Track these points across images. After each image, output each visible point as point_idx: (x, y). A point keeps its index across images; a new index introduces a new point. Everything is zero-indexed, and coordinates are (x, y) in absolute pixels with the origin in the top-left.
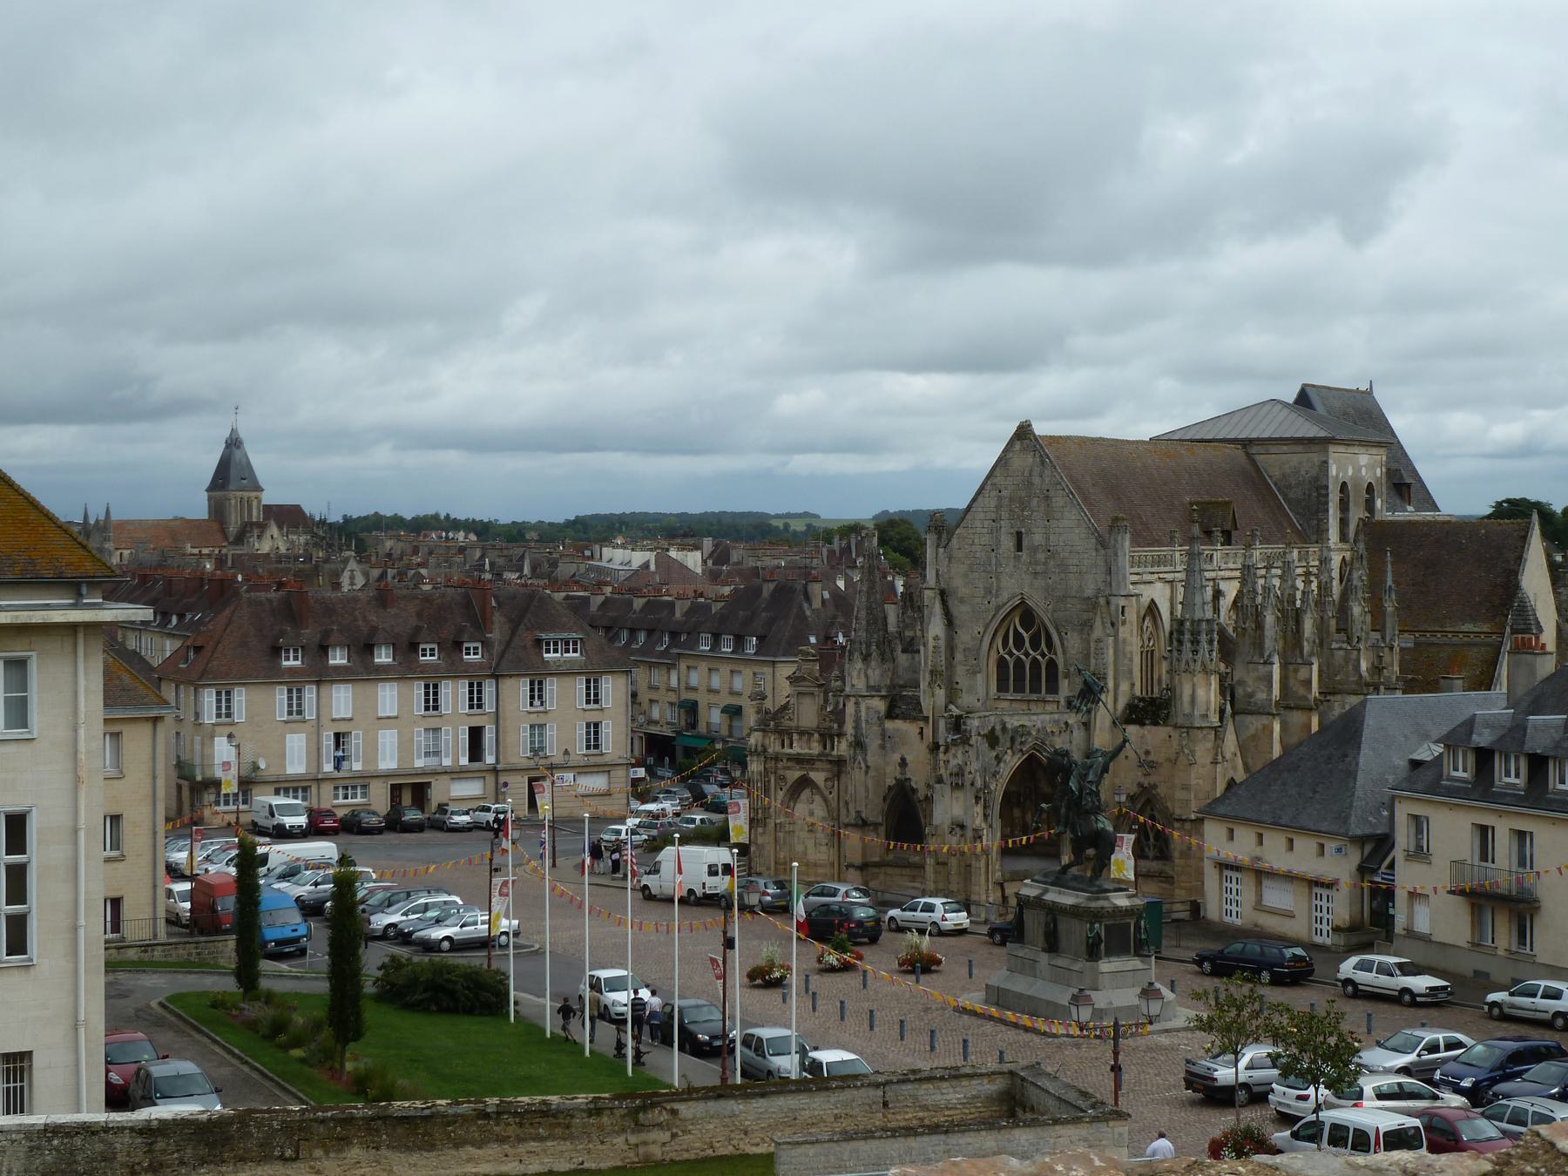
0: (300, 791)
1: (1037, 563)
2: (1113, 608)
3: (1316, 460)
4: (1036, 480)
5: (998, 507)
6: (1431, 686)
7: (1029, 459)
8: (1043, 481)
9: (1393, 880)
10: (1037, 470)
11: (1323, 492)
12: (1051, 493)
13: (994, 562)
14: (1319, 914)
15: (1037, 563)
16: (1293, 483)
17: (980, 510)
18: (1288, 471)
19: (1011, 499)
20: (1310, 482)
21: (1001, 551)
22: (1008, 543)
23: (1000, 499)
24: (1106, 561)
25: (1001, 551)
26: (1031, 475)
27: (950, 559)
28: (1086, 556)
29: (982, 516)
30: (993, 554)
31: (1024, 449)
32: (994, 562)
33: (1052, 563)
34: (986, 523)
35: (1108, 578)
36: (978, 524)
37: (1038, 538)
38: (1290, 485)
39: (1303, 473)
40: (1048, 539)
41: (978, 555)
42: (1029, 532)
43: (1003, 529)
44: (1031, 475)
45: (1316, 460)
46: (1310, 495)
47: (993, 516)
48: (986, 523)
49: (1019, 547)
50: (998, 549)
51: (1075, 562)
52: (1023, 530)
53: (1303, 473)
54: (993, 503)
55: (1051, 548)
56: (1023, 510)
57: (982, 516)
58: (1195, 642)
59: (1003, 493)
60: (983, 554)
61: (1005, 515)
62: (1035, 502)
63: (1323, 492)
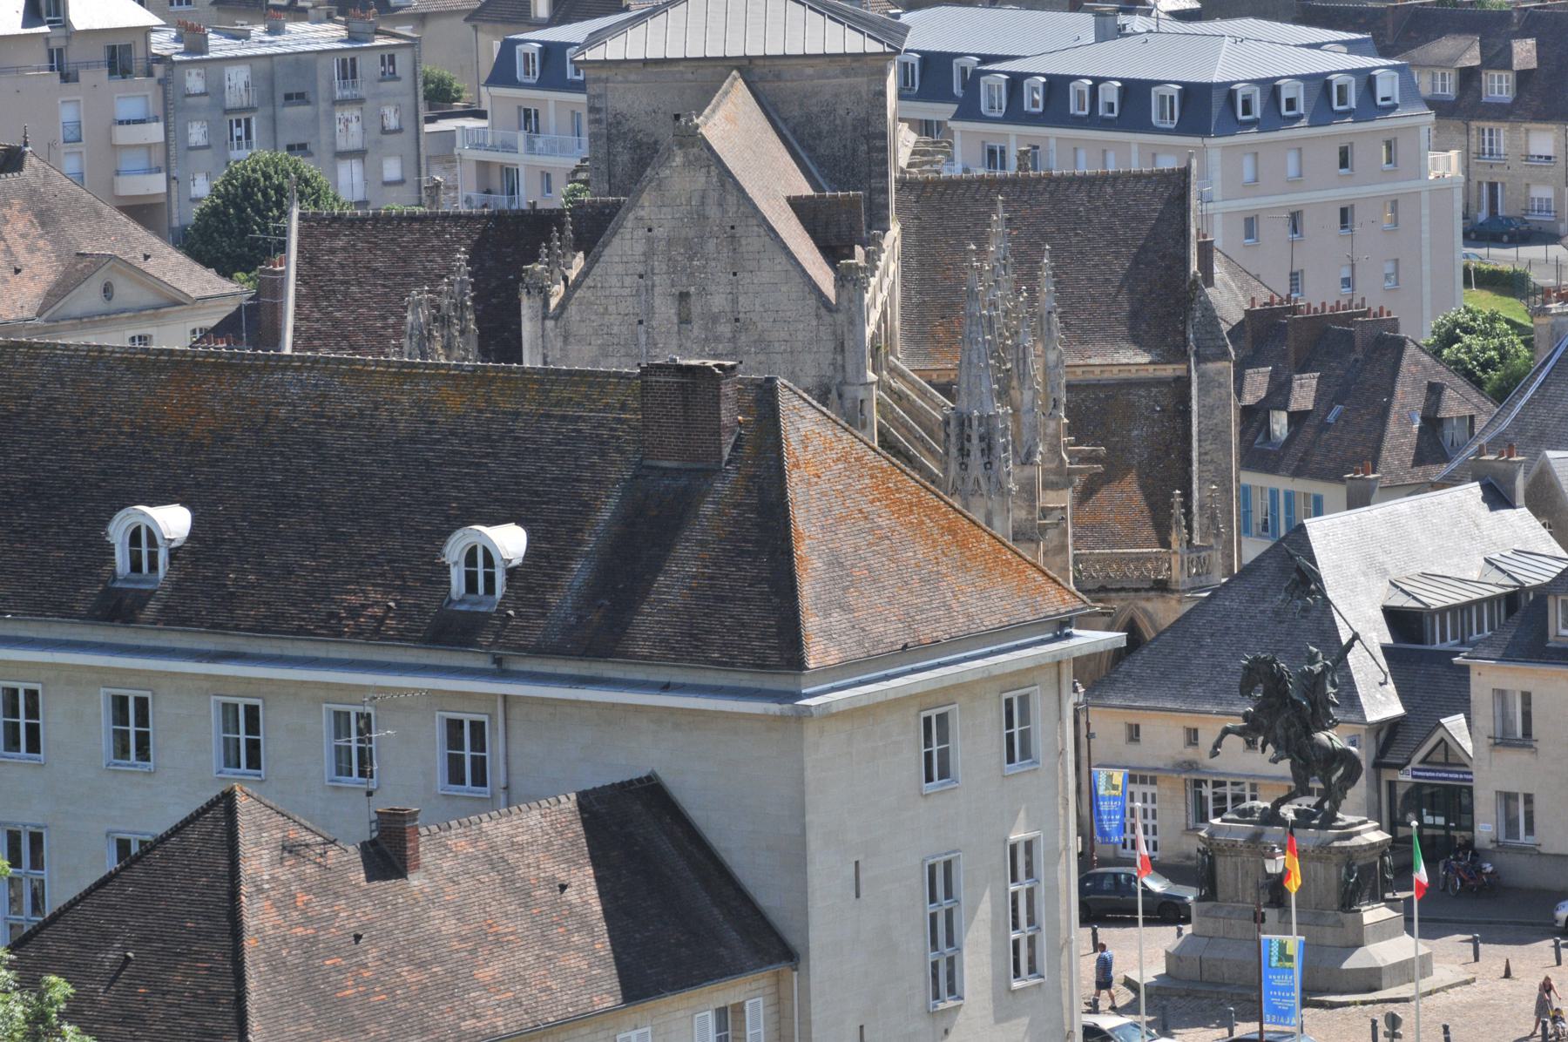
0: (1242, 806)
1: (717, 339)
2: (848, 404)
3: (864, 89)
4: (713, 212)
5: (648, 255)
6: (1366, 502)
7: (700, 180)
8: (725, 212)
9: (1471, 780)
10: (713, 196)
11: (878, 143)
12: (739, 231)
13: (643, 339)
14: (1129, 836)
15: (717, 339)
16: (825, 128)
17: (617, 259)
18: (815, 109)
19: (670, 242)
20: (855, 128)
21: (654, 323)
22: (665, 310)
23: (650, 241)
24: (834, 333)
25: (654, 323)
26: (703, 204)
27: (566, 339)
28: (801, 326)
29: (620, 268)
30: (642, 328)
31: (690, 163)
32: (643, 339)
33: (743, 338)
34: (628, 281)
35: (839, 358)
36: (614, 281)
37: (719, 302)
38: (819, 133)
39: (841, 112)
40: (735, 301)
41: (615, 330)
42: (703, 291)
43: (657, 290)
44: (703, 204)
45: (864, 89)
46: (854, 151)
47: (640, 269)
48: (628, 281)
49: (685, 320)
50: (649, 320)
51: (784, 335)
52: (692, 289)
53: (841, 112)
54: (640, 248)
55: (741, 316)
56: (691, 259)
57: (620, 268)
58: (988, 450)
59: (655, 232)
60: (624, 329)
61: (659, 265)
62: (711, 245)
63: (878, 143)
